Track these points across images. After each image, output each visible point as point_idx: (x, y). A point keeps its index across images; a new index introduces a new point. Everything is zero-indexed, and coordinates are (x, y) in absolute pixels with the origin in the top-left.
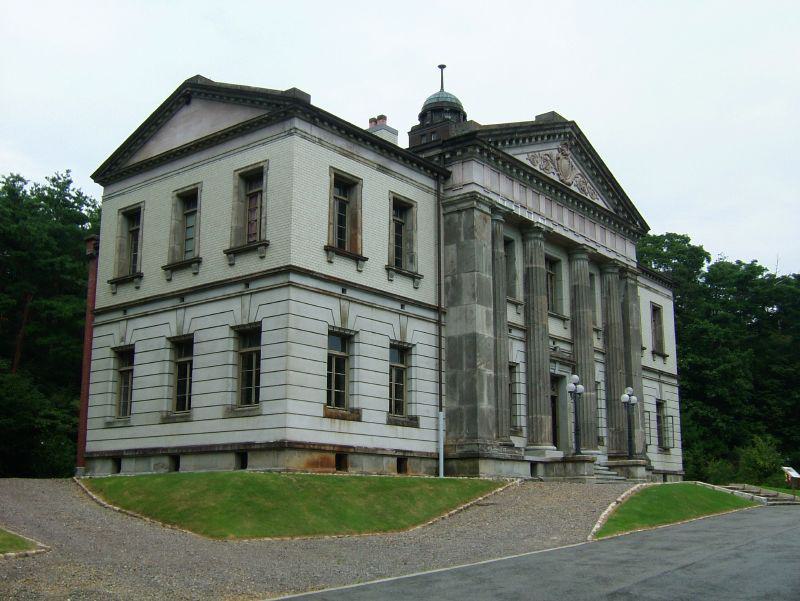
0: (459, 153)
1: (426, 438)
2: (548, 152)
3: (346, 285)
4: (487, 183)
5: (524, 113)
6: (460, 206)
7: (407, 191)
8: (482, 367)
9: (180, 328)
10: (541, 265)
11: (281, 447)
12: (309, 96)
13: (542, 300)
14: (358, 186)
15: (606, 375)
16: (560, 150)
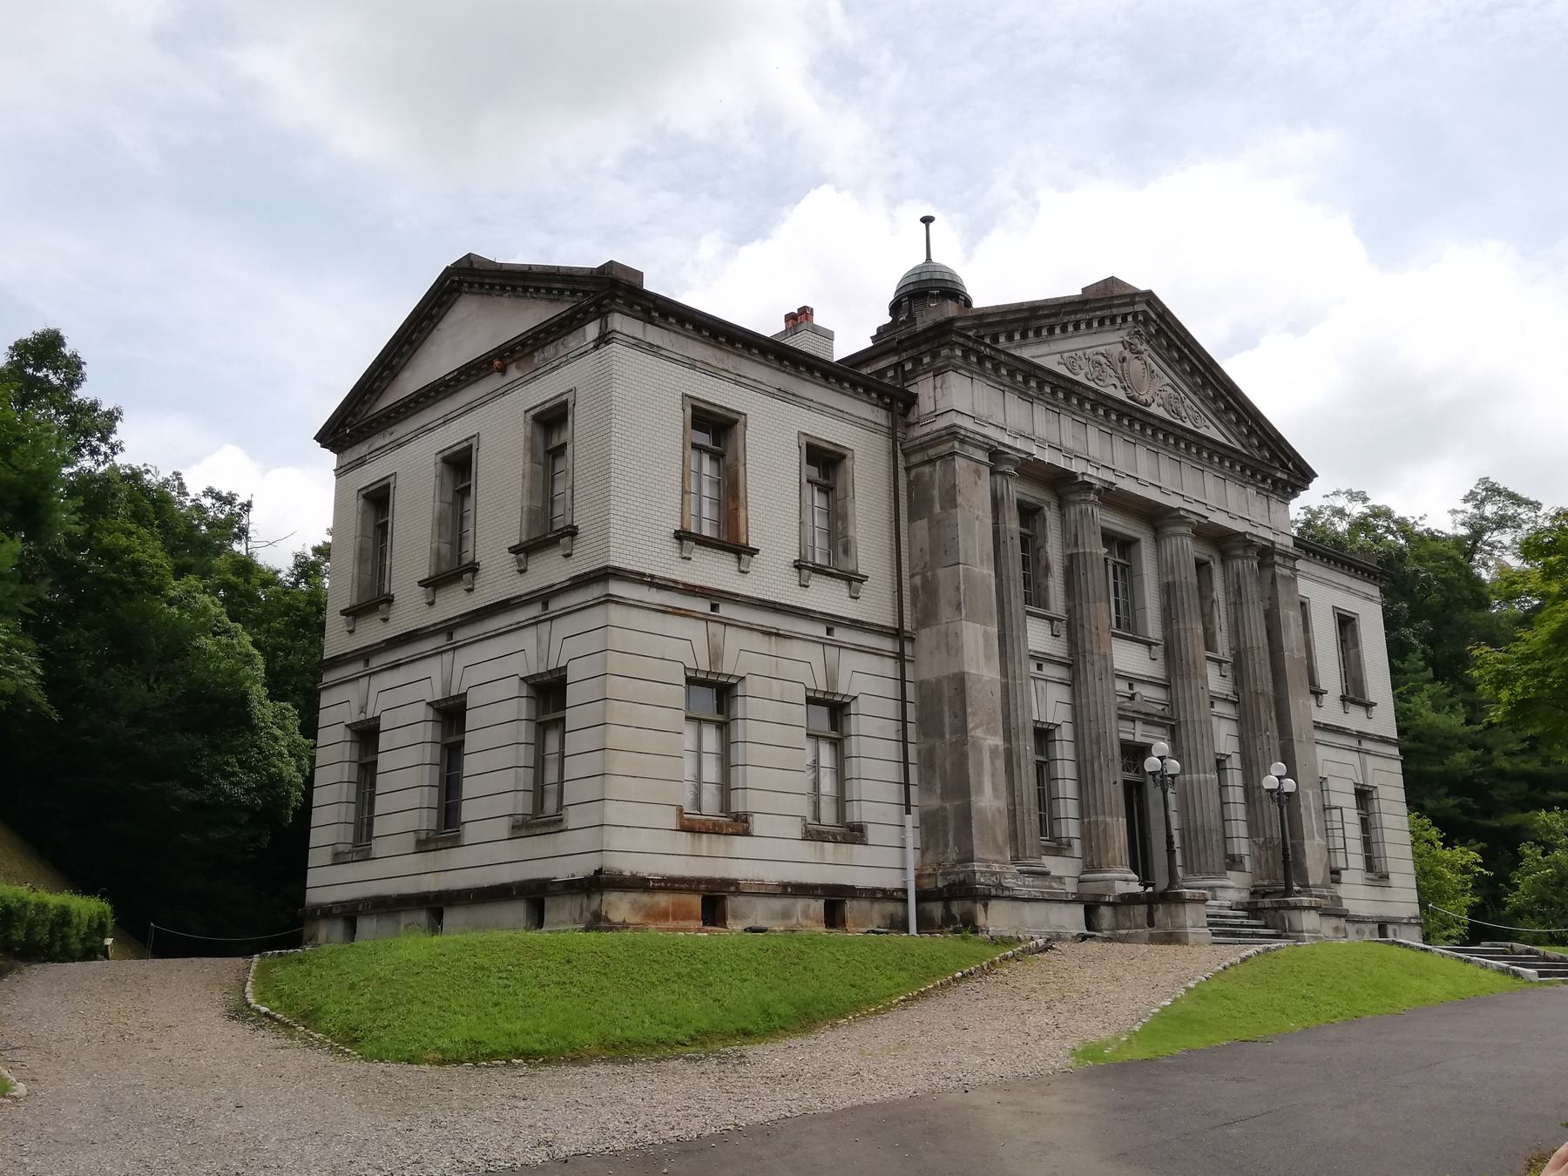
0: (926, 360)
1: (885, 860)
2: (1101, 349)
3: (716, 597)
4: (981, 410)
5: (1062, 280)
6: (932, 452)
7: (832, 432)
8: (979, 733)
9: (447, 684)
10: (1189, 576)
11: (600, 883)
12: (640, 275)
13: (1102, 613)
14: (739, 427)
15: (1241, 742)
16: (1128, 345)
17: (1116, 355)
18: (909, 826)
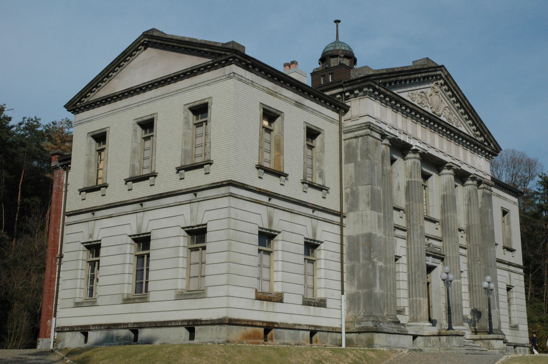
3: (271, 195)
7: (317, 122)
9: (139, 227)
12: (244, 48)
17: (428, 94)
18: (343, 300)
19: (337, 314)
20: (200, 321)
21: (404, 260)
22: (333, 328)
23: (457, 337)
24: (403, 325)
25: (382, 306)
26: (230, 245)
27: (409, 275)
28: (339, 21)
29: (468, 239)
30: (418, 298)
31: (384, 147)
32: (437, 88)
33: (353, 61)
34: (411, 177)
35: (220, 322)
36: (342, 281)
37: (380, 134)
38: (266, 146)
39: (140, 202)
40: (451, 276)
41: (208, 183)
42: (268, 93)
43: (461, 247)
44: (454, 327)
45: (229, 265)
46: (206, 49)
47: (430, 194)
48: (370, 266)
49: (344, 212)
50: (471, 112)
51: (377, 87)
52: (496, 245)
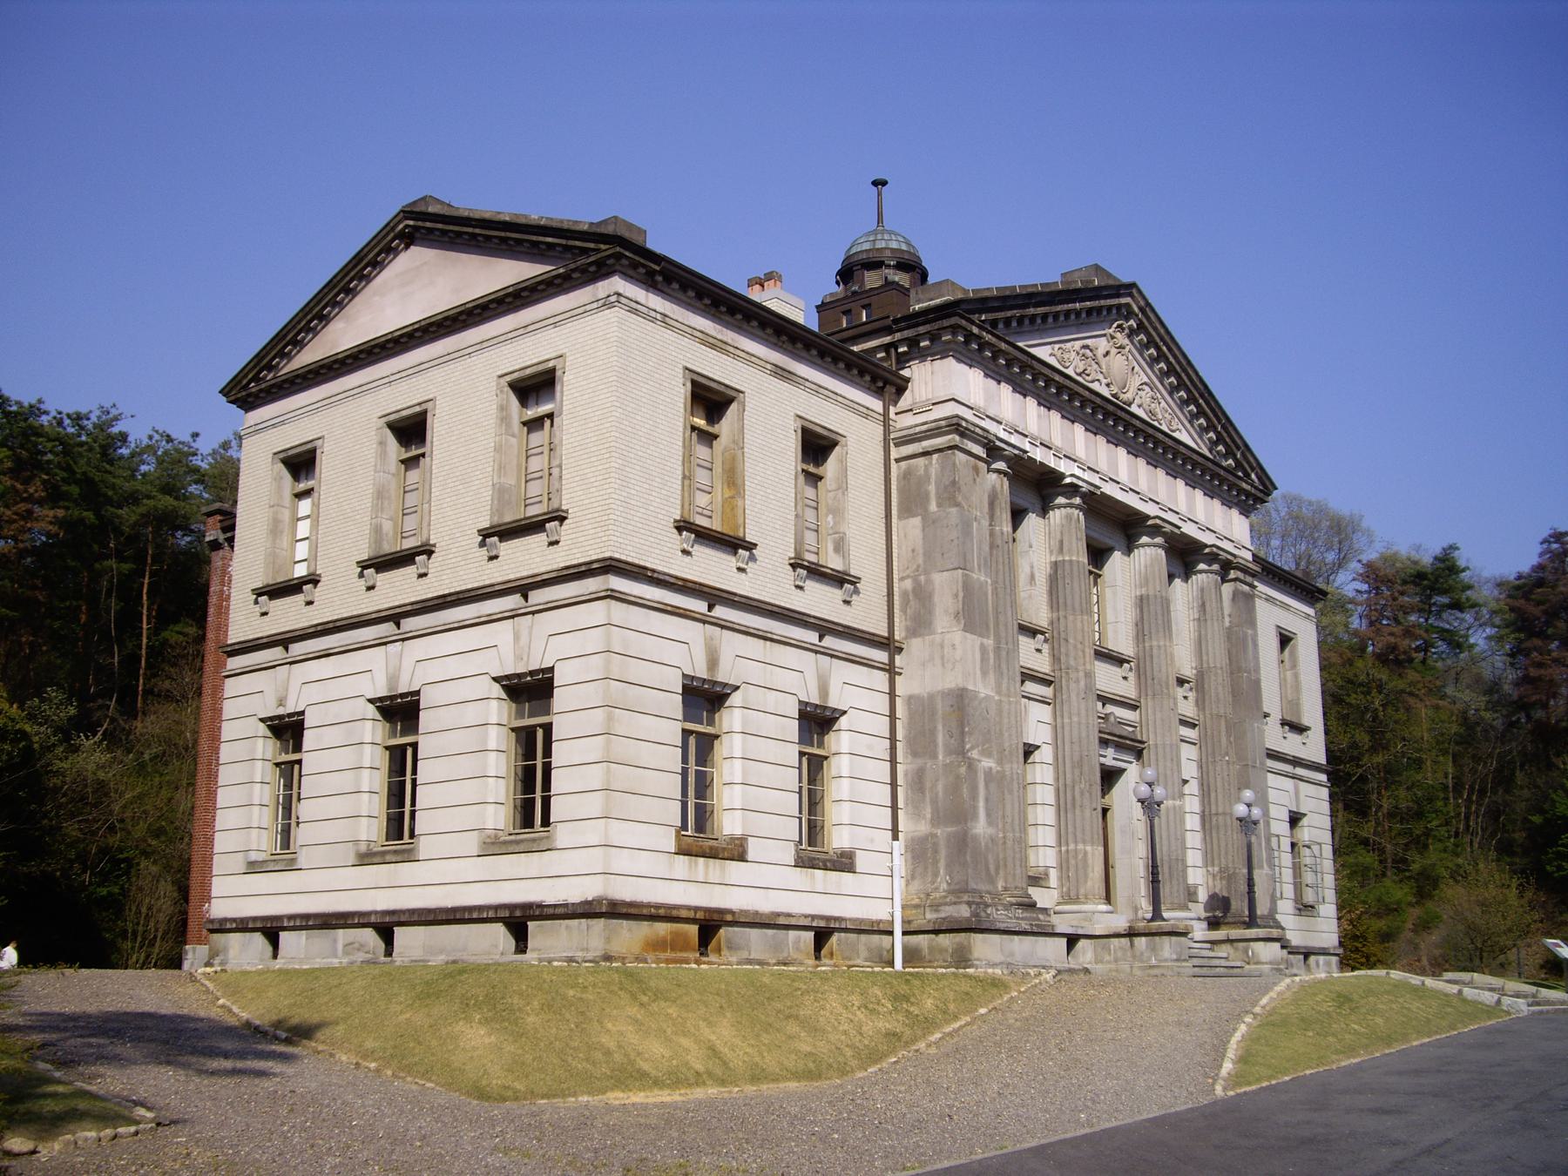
3: (714, 596)
7: (827, 417)
9: (393, 679)
19: (880, 886)
20: (540, 906)
21: (1045, 754)
22: (872, 922)
23: (1174, 939)
24: (1045, 910)
25: (992, 867)
26: (610, 718)
27: (1058, 790)
28: (884, 183)
29: (1200, 704)
30: (1080, 846)
31: (994, 481)
32: (1121, 338)
33: (918, 276)
34: (1061, 550)
35: (586, 911)
36: (894, 808)
37: (984, 446)
38: (702, 477)
39: (396, 617)
40: (1159, 792)
41: (555, 567)
42: (704, 343)
43: (1184, 723)
44: (1165, 915)
45: (608, 770)
46: (550, 240)
47: (1108, 593)
48: (963, 770)
49: (897, 637)
50: (1202, 396)
51: (975, 330)
52: (1266, 715)
